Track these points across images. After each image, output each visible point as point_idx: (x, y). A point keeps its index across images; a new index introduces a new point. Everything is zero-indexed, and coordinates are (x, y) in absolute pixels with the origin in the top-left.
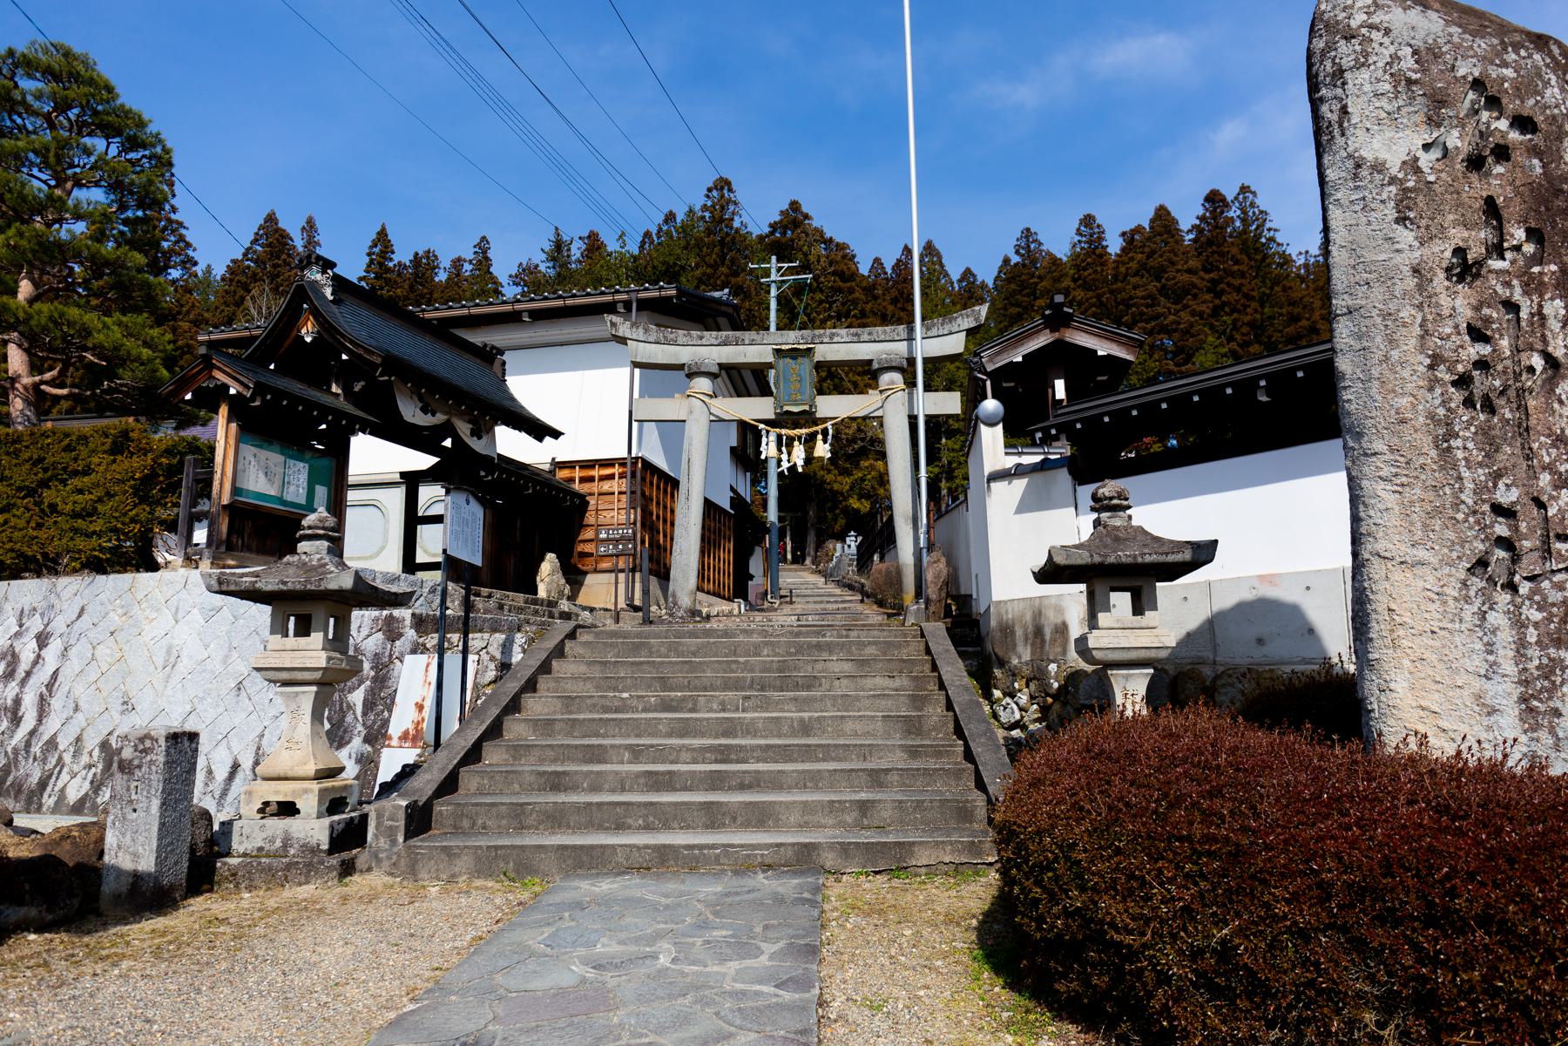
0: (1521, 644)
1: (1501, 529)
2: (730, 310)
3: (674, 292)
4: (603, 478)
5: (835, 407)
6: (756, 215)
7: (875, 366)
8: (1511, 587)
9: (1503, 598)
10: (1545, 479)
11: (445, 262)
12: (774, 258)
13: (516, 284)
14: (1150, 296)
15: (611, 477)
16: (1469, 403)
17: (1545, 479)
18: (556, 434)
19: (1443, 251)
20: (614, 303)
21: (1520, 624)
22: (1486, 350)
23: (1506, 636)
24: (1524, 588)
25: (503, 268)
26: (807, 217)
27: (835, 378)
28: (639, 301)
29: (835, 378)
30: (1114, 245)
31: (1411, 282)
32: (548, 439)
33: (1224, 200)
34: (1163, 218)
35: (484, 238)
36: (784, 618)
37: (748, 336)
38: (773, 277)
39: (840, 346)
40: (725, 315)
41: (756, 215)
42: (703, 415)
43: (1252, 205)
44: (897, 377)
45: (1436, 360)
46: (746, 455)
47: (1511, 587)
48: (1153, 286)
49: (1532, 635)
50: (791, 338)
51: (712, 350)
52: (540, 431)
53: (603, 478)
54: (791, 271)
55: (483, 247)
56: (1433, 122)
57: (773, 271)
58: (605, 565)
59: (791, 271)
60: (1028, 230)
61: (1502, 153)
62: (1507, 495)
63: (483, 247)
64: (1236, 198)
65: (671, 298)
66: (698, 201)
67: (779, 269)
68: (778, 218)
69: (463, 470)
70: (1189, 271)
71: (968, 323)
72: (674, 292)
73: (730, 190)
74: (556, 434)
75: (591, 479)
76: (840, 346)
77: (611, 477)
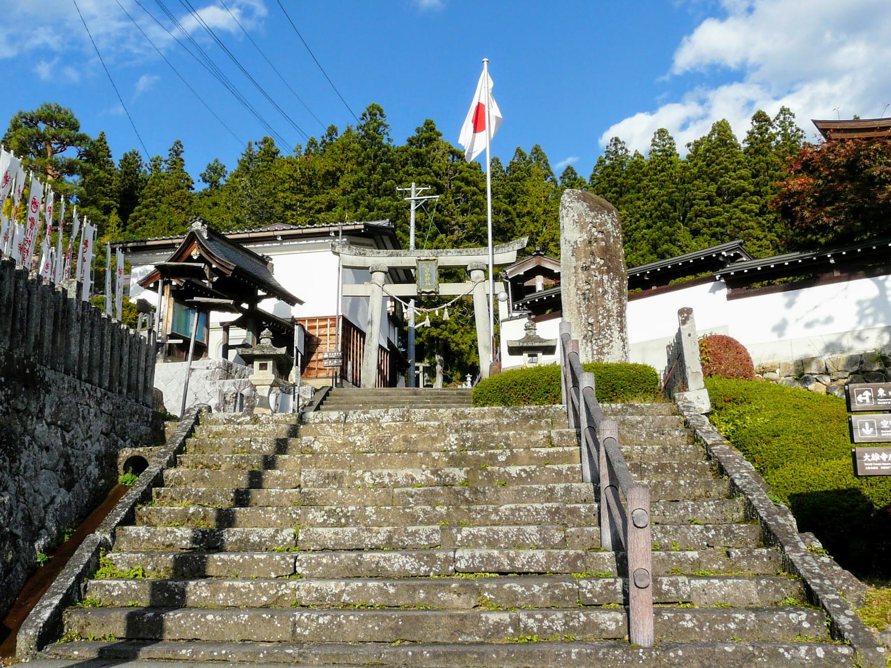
0: (593, 354)
1: (589, 328)
2: (390, 231)
3: (362, 227)
4: (320, 327)
5: (448, 289)
6: (398, 135)
7: (469, 268)
8: (591, 342)
9: (590, 344)
10: (600, 317)
11: (146, 160)
12: (413, 184)
13: (205, 181)
14: (709, 197)
15: (326, 326)
16: (584, 299)
17: (600, 317)
18: (301, 303)
19: (581, 263)
20: (329, 232)
21: (592, 350)
22: (589, 287)
23: (590, 353)
24: (594, 342)
25: (194, 169)
26: (439, 135)
27: (450, 274)
28: (343, 231)
29: (450, 274)
30: (682, 151)
31: (573, 270)
32: (297, 305)
33: (767, 120)
34: (722, 129)
35: (178, 143)
36: (409, 471)
37: (402, 252)
38: (413, 197)
39: (451, 258)
40: (386, 234)
41: (398, 135)
42: (377, 296)
43: (791, 124)
44: (480, 273)
45: (578, 289)
46: (396, 320)
47: (591, 342)
48: (713, 188)
49: (595, 352)
50: (426, 253)
51: (384, 259)
52: (292, 300)
53: (320, 327)
54: (424, 193)
55: (177, 151)
56: (581, 232)
57: (413, 193)
58: (321, 374)
59: (424, 193)
60: (617, 139)
61: (596, 240)
62: (591, 320)
63: (177, 151)
64: (777, 118)
65: (360, 230)
66: (355, 123)
67: (417, 192)
68: (415, 134)
69: (254, 321)
70: (741, 178)
71: (518, 247)
72: (362, 227)
73: (382, 115)
74: (301, 303)
75: (315, 327)
76: (451, 258)
77: (326, 326)
